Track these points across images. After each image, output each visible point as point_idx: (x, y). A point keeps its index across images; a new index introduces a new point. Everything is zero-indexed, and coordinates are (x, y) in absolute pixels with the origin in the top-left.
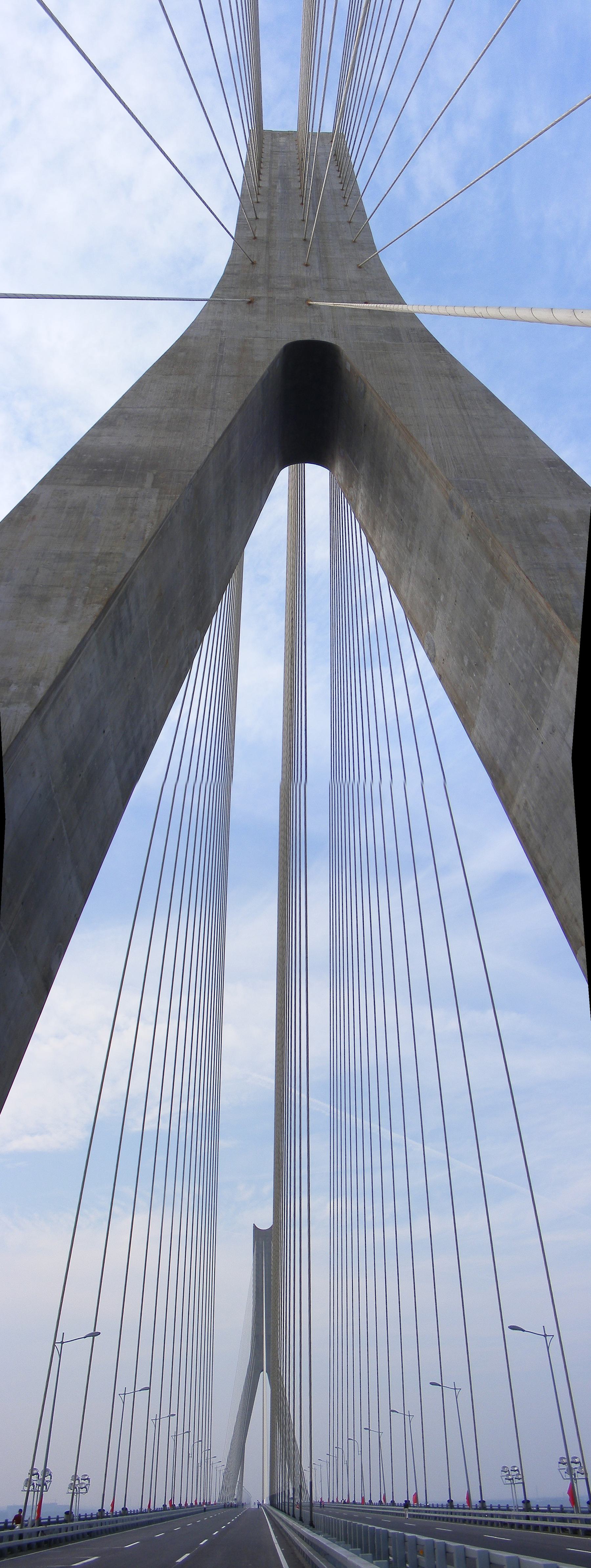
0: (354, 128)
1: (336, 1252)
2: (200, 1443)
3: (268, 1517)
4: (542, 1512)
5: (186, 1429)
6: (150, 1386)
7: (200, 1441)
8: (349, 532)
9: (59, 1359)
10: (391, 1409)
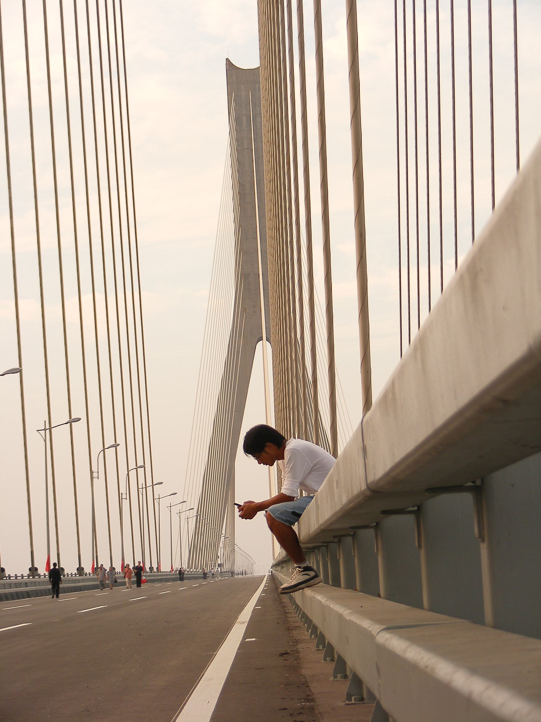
0: (218, 248)
1: (202, 421)
2: (141, 471)
3: (292, 425)
4: (298, 400)
5: (109, 441)
6: (144, 464)
7: (141, 467)
8: (222, 294)
9: (170, 513)
10: (138, 469)
